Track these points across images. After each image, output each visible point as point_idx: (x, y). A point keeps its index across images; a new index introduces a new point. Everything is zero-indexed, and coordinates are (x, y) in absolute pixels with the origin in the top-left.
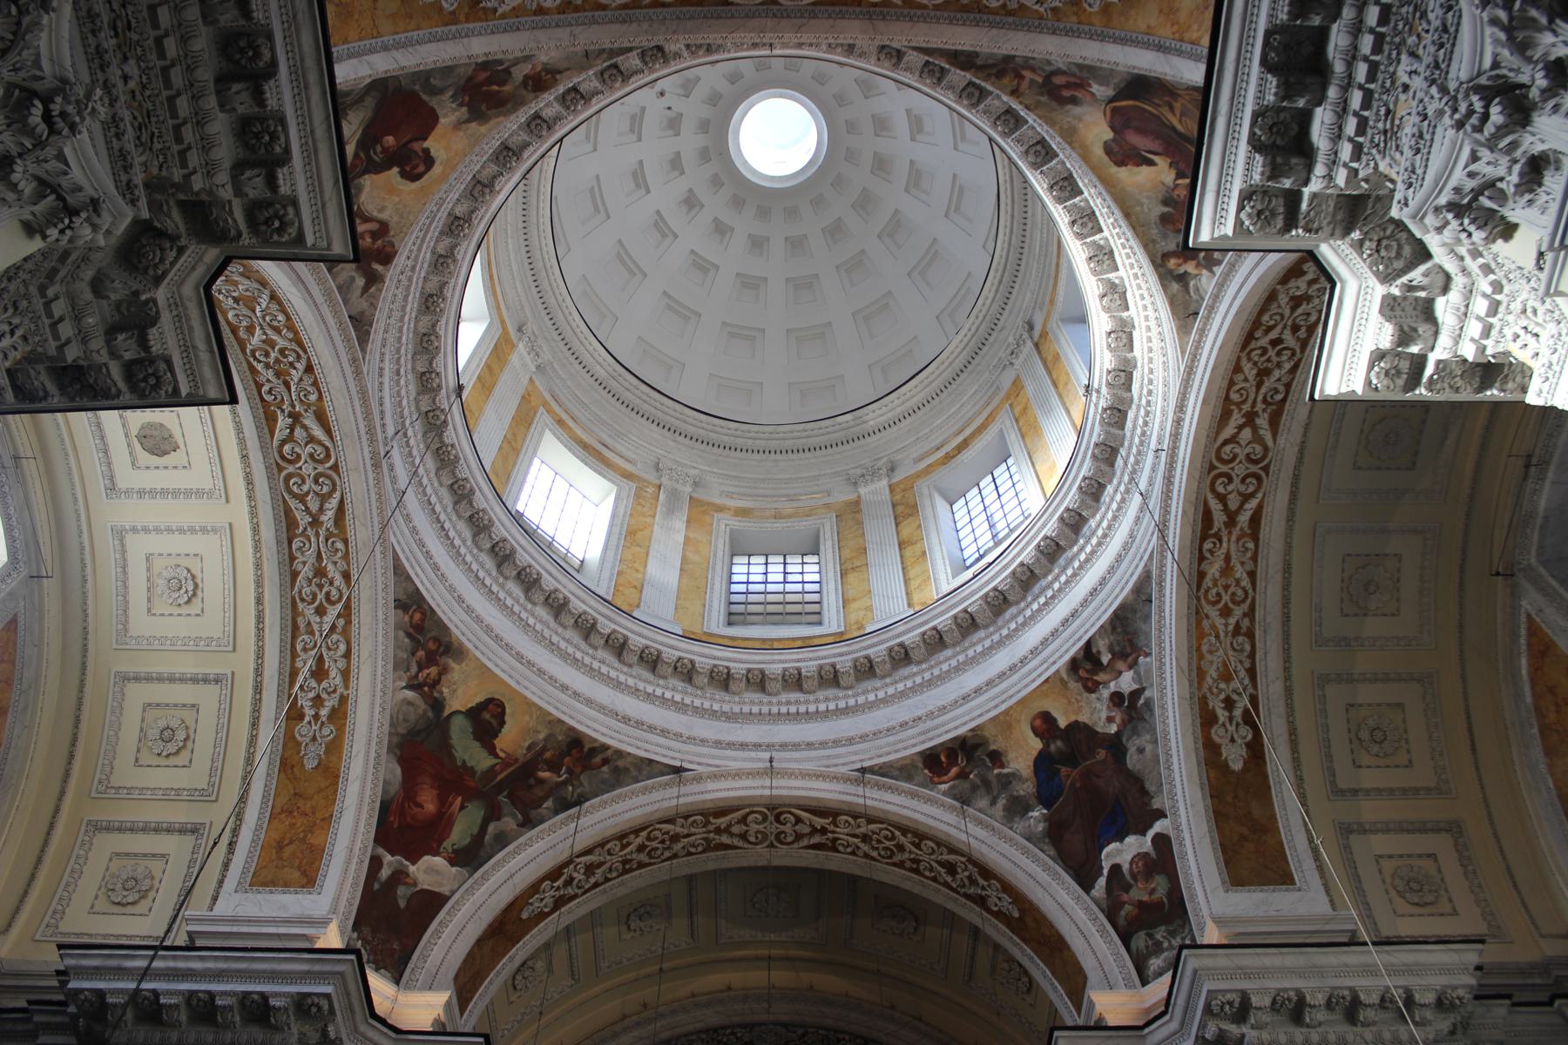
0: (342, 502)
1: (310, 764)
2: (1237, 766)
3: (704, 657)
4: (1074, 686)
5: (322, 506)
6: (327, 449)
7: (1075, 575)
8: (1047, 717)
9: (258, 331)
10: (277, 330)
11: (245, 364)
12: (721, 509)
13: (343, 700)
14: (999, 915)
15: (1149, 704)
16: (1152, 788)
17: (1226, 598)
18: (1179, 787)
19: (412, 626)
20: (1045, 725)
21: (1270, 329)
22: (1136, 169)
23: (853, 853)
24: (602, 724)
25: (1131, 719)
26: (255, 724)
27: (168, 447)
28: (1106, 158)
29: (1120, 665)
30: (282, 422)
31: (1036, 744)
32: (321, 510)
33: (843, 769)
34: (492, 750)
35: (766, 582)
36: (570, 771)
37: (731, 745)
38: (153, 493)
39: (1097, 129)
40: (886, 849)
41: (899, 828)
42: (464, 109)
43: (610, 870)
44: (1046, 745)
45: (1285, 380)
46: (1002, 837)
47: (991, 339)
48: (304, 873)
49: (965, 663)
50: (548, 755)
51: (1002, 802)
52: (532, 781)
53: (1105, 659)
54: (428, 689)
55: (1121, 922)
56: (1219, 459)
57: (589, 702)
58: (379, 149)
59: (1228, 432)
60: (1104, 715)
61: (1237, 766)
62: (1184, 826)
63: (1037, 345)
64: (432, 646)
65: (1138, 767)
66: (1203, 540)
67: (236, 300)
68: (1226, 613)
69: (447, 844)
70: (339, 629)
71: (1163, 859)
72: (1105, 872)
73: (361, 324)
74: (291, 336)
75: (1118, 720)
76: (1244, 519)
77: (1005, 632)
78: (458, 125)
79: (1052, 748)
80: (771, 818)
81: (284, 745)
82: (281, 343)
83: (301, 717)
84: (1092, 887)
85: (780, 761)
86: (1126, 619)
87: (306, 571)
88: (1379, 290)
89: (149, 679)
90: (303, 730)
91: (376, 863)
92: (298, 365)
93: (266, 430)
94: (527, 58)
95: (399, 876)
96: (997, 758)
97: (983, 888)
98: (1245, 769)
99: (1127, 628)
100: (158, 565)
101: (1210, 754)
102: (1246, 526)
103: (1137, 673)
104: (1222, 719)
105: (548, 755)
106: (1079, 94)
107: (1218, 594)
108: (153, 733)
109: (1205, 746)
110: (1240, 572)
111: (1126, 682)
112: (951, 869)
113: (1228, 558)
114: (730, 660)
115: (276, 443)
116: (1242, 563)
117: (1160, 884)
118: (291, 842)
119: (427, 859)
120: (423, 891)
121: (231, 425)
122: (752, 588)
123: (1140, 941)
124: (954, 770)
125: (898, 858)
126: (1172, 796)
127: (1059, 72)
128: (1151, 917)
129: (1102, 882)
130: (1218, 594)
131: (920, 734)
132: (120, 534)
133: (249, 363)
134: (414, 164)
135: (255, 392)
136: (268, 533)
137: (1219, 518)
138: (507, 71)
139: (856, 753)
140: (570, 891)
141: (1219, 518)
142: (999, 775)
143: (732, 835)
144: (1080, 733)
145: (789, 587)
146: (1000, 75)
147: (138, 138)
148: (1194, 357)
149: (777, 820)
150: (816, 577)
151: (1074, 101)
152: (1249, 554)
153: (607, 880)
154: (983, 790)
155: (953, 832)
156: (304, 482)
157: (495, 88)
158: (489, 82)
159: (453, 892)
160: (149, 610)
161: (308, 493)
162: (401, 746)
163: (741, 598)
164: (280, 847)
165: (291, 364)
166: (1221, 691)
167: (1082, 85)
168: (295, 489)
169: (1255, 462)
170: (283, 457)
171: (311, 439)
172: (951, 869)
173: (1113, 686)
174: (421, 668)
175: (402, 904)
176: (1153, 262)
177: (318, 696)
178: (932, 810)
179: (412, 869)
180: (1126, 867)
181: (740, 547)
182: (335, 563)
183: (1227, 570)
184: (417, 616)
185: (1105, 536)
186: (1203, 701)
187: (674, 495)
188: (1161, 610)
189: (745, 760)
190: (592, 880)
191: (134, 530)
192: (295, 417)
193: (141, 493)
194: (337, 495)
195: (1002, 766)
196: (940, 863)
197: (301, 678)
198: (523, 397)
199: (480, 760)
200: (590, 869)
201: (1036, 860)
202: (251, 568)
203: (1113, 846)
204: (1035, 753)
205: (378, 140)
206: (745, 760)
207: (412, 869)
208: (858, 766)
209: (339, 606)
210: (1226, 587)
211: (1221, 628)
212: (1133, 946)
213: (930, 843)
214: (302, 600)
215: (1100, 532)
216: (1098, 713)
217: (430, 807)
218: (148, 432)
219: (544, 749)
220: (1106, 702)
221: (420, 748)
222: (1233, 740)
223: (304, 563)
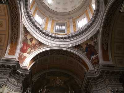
4: (90, 40)
8: (88, 44)
20: (87, 44)
29: (95, 39)
96: (82, 47)
99: (96, 36)
111: (95, 41)
112: (76, 57)
123: (94, 65)
216: (92, 43)
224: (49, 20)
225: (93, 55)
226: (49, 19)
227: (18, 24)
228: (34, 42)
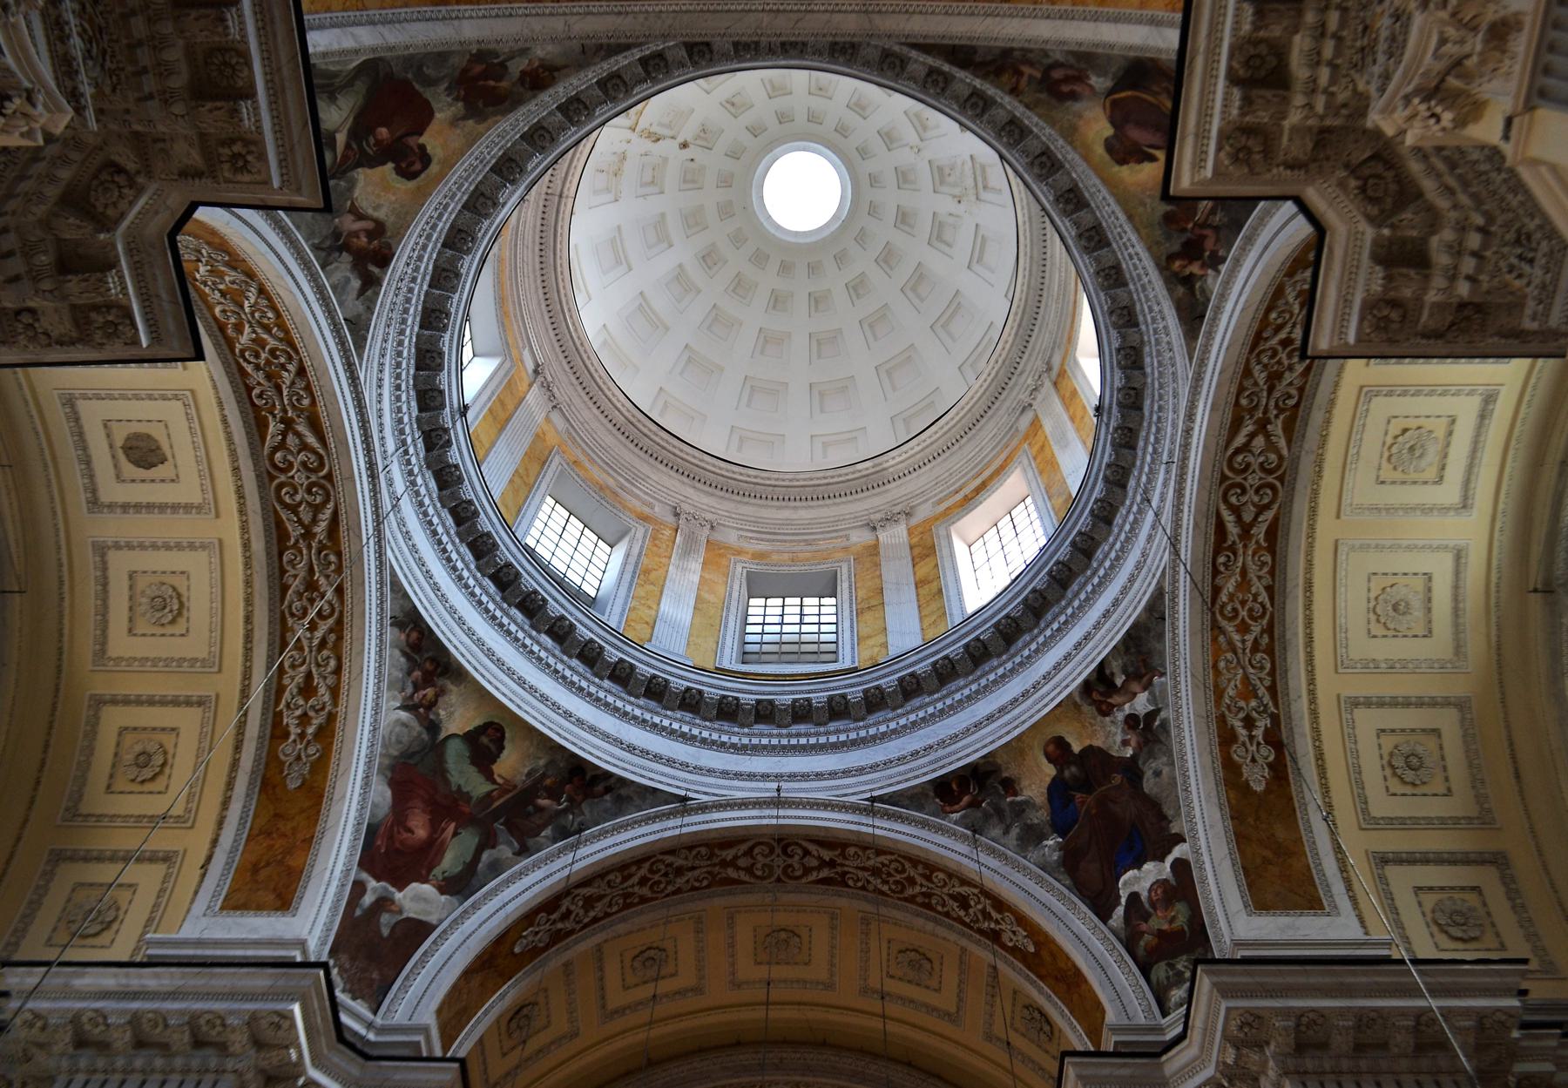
1: (293, 784)
2: (1259, 788)
3: (712, 689)
4: (1088, 709)
6: (321, 457)
7: (1087, 599)
8: (1060, 743)
9: (247, 329)
10: (267, 329)
11: (234, 366)
12: (739, 552)
13: (331, 717)
14: (1014, 951)
15: (1164, 725)
16: (1170, 813)
17: (1244, 613)
18: (1197, 809)
19: (408, 644)
20: (1059, 751)
21: (1279, 328)
22: (1138, 167)
23: (863, 888)
24: (605, 752)
26: (238, 747)
27: (155, 460)
28: (1107, 157)
29: (1135, 686)
30: (273, 427)
31: (1050, 771)
32: (315, 521)
33: (853, 799)
34: (490, 777)
35: (782, 624)
36: (570, 799)
37: (738, 776)
38: (138, 507)
39: (1097, 126)
40: (896, 882)
41: (910, 859)
42: (460, 104)
43: (610, 905)
44: (1060, 771)
45: (1298, 383)
46: (1017, 866)
47: (1011, 383)
48: (279, 896)
49: (977, 692)
50: (548, 782)
51: (1015, 831)
52: (530, 808)
53: (1119, 681)
54: (422, 709)
55: (1141, 952)
56: (1231, 467)
57: (593, 730)
58: (372, 141)
59: (1240, 440)
60: (1119, 738)
61: (1259, 788)
62: (1204, 850)
63: (1055, 384)
64: (428, 666)
65: (1155, 790)
67: (223, 294)
68: (1244, 629)
69: (437, 871)
70: (330, 644)
71: (1183, 885)
72: (1123, 901)
73: (358, 328)
74: (282, 335)
75: (1133, 743)
76: (1260, 532)
77: (1018, 659)
78: (455, 122)
79: (1067, 774)
80: (778, 851)
81: (267, 764)
82: (272, 343)
83: (287, 735)
84: (1110, 917)
85: (788, 791)
87: (296, 585)
88: (1369, 233)
89: (126, 701)
90: (287, 750)
91: (359, 888)
92: (290, 367)
93: (257, 437)
94: (524, 51)
95: (383, 903)
96: (1010, 786)
97: (997, 922)
98: (1268, 790)
99: (1140, 650)
100: (142, 583)
101: (1230, 775)
103: (1152, 694)
105: (548, 782)
106: (1077, 88)
107: (1235, 610)
108: (128, 758)
109: (1225, 766)
110: (1257, 586)
111: (1141, 703)
112: (964, 902)
113: (1244, 572)
114: (739, 691)
115: (266, 451)
116: (1260, 578)
117: (1181, 912)
118: (268, 864)
119: (415, 887)
120: (408, 919)
121: (222, 436)
122: (767, 629)
123: (1160, 971)
124: (966, 799)
125: (909, 892)
126: (1191, 820)
127: (1057, 65)
128: (1171, 944)
129: (1120, 911)
130: (1235, 610)
131: (931, 763)
132: (101, 550)
133: (238, 364)
134: (412, 163)
135: (245, 395)
136: (258, 546)
138: (503, 65)
139: (866, 783)
140: (568, 925)
142: (1012, 803)
143: (738, 868)
144: (1095, 757)
145: (805, 628)
146: (998, 72)
147: (89, 51)
148: (1202, 363)
149: (785, 852)
150: (833, 619)
151: (1074, 96)
152: (1266, 569)
153: (607, 915)
154: (995, 819)
155: (965, 861)
156: (296, 492)
157: (492, 83)
158: (485, 75)
159: (441, 921)
160: (130, 630)
161: (300, 504)
162: (393, 768)
163: (756, 648)
164: (256, 869)
165: (283, 367)
166: (1241, 709)
167: (1080, 78)
168: (287, 499)
169: (1270, 472)
170: (275, 466)
171: (304, 447)
172: (964, 902)
174: (416, 688)
175: (385, 932)
176: (1158, 265)
177: (305, 714)
178: (942, 841)
179: (398, 896)
180: (1144, 895)
181: (759, 586)
182: (327, 577)
184: (414, 635)
185: (1117, 558)
186: (1222, 719)
187: (691, 541)
188: (1174, 628)
189: (752, 790)
190: (592, 914)
191: (117, 546)
192: (288, 424)
193: (125, 507)
194: (331, 505)
195: (1016, 795)
196: (952, 896)
197: (287, 695)
198: (537, 435)
199: (475, 785)
200: (589, 902)
201: (1050, 889)
202: (241, 585)
203: (1130, 874)
204: (1048, 780)
205: (371, 130)
206: (752, 790)
207: (398, 896)
208: (868, 795)
209: (331, 621)
210: (1243, 603)
212: (1153, 978)
213: (941, 875)
214: (293, 615)
215: (1113, 555)
216: (1113, 737)
217: (421, 833)
218: (135, 443)
219: (544, 776)
220: (1120, 725)
221: (413, 773)
222: (1253, 760)
223: (295, 576)
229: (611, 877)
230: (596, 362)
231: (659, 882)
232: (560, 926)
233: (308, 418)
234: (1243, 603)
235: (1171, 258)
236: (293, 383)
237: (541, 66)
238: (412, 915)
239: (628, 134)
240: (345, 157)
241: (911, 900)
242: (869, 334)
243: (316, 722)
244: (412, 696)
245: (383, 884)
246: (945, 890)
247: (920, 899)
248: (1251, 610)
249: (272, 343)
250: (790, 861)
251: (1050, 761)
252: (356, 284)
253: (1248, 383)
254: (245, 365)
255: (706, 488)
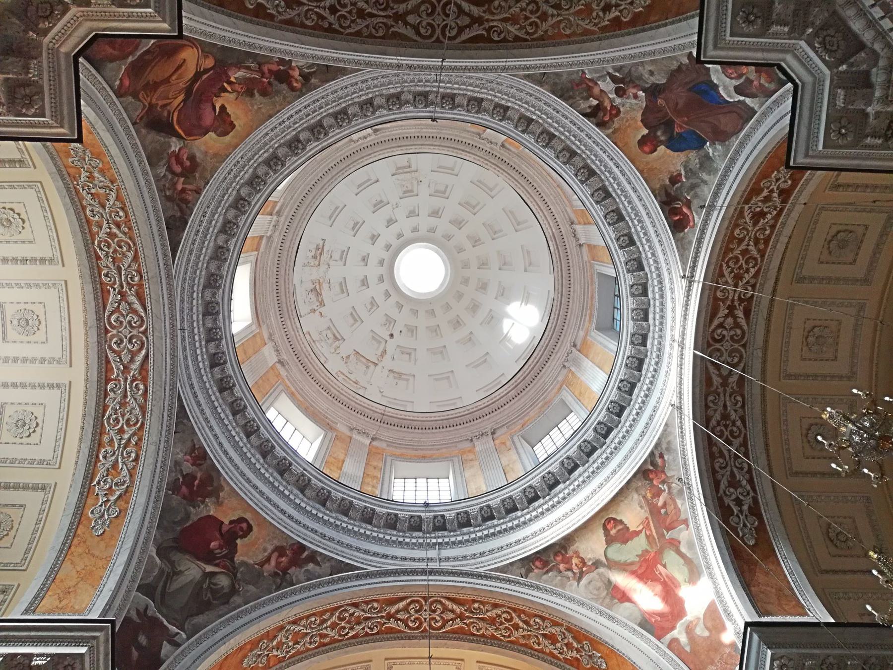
0: (448, 599)
4: (617, 123)
5: (450, 611)
6: (412, 602)
8: (642, 142)
20: (648, 143)
25: (631, 81)
29: (596, 91)
34: (637, 533)
36: (663, 482)
44: (662, 143)
50: (649, 495)
51: (705, 176)
52: (663, 511)
53: (595, 102)
55: (772, 86)
56: (431, 36)
59: (410, 32)
60: (634, 101)
64: (559, 558)
66: (491, 41)
72: (742, 98)
74: (328, 614)
75: (634, 91)
78: (219, 503)
79: (662, 138)
83: (577, 659)
84: (752, 109)
86: (562, 89)
87: (491, 630)
92: (351, 611)
96: (675, 179)
97: (772, 191)
99: (571, 89)
102: (482, 9)
103: (599, 78)
104: (617, 13)
107: (531, 24)
111: (607, 86)
113: (505, 20)
124: (685, 210)
129: (748, 101)
130: (531, 24)
135: (371, 638)
137: (477, 31)
141: (477, 31)
148: (358, 63)
151: (192, 158)
154: (697, 190)
156: (435, 618)
157: (196, 482)
158: (190, 485)
170: (418, 628)
171: (406, 609)
173: (612, 96)
174: (570, 569)
177: (566, 645)
183: (513, 20)
190: (744, 482)
192: (389, 616)
194: (443, 600)
195: (680, 175)
197: (555, 652)
204: (668, 151)
205: (211, 551)
210: (527, 18)
211: (555, 20)
214: (509, 636)
216: (634, 105)
219: (644, 497)
220: (624, 100)
223: (487, 629)
224: (579, 375)
225: (715, 87)
226: (573, 373)
227: (496, 606)
228: (632, 515)
229: (717, 466)
230: (479, 403)
231: (732, 432)
232: (745, 507)
233: (387, 605)
234: (527, 18)
235: (293, 89)
236: (363, 610)
237: (190, 455)
238: (703, 612)
239: (379, 368)
240: (223, 568)
241: (762, 254)
242: (499, 234)
243: (571, 640)
244: (574, 573)
245: (678, 625)
246: (750, 228)
247: (762, 247)
248: (531, 12)
249: (334, 618)
250: (727, 338)
251: (655, 150)
252: (311, 566)
253: (365, 32)
254: (349, 635)
255: (558, 345)
